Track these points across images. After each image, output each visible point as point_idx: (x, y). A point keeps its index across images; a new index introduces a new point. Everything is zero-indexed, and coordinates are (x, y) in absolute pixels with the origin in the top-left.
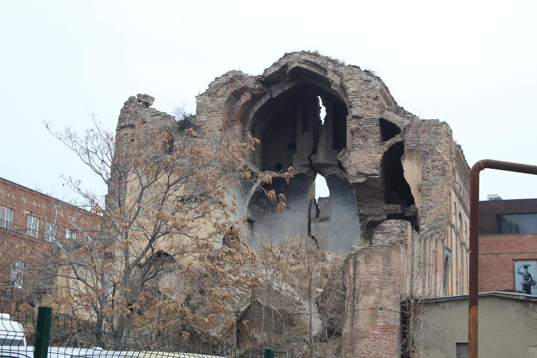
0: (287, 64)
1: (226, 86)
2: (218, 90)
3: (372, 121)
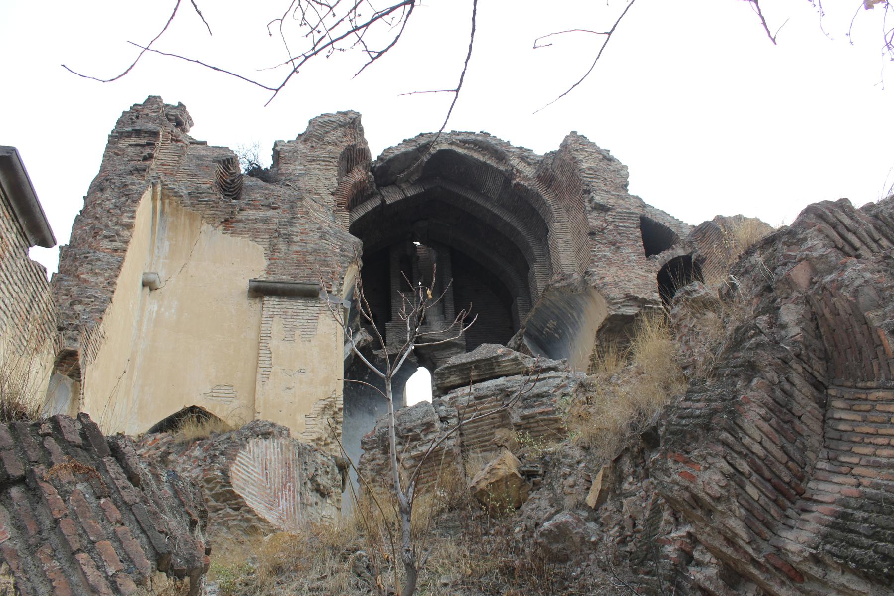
0: (428, 143)
1: (342, 129)
2: (327, 132)
3: (630, 218)
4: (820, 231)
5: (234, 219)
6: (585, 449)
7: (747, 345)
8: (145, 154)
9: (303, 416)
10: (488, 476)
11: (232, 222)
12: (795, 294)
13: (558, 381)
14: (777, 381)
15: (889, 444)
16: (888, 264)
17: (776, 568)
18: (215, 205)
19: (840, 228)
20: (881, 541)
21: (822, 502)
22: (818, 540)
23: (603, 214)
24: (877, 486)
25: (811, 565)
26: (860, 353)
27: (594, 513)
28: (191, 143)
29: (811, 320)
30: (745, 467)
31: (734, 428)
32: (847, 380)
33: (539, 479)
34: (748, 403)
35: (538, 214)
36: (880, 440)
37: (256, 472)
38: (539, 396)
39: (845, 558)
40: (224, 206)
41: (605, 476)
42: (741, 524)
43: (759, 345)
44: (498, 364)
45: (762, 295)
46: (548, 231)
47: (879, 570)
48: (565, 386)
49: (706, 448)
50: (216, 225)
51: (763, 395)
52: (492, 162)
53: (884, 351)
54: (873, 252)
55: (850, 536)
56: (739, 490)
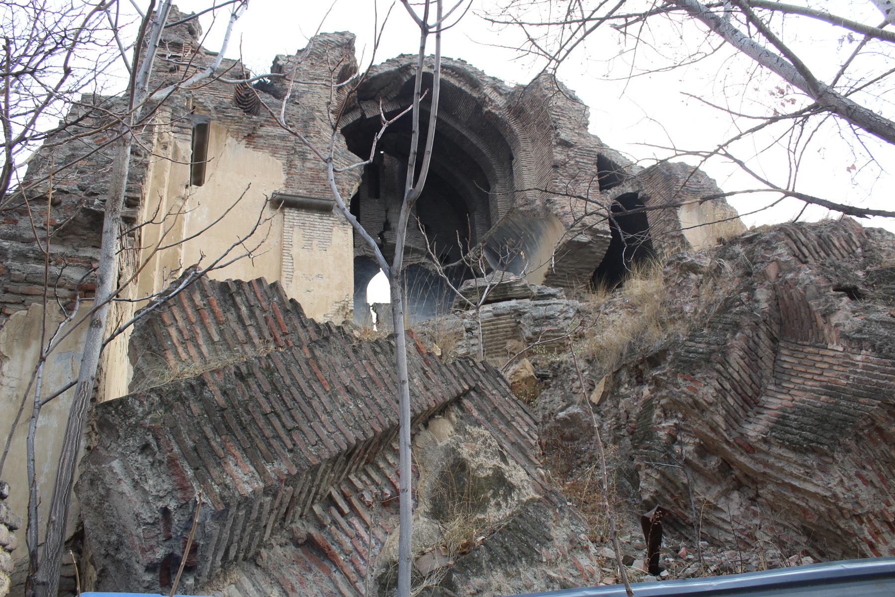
0: (409, 65)
1: (340, 49)
3: (589, 155)
4: (787, 244)
5: (256, 135)
6: (589, 362)
7: (734, 310)
9: (322, 316)
10: (513, 376)
11: (254, 137)
12: (767, 283)
13: (561, 307)
14: (751, 335)
15: (812, 379)
16: (823, 269)
17: (739, 445)
18: (239, 121)
19: (799, 243)
20: (803, 431)
21: (770, 409)
22: (767, 430)
23: (566, 150)
24: (804, 402)
25: (762, 444)
26: (802, 324)
27: (597, 407)
28: (207, 54)
29: (775, 300)
30: (727, 386)
31: (725, 362)
32: (792, 338)
33: (549, 380)
34: (733, 347)
35: (504, 139)
36: (808, 376)
38: (548, 318)
39: (783, 440)
40: (247, 122)
41: (606, 383)
42: (722, 419)
43: (742, 313)
44: (511, 289)
45: (743, 277)
46: (512, 158)
47: (802, 446)
48: (566, 311)
49: (706, 374)
50: (239, 139)
51: (742, 343)
52: (466, 89)
53: (817, 326)
54: (815, 259)
55: (786, 428)
56: (724, 400)
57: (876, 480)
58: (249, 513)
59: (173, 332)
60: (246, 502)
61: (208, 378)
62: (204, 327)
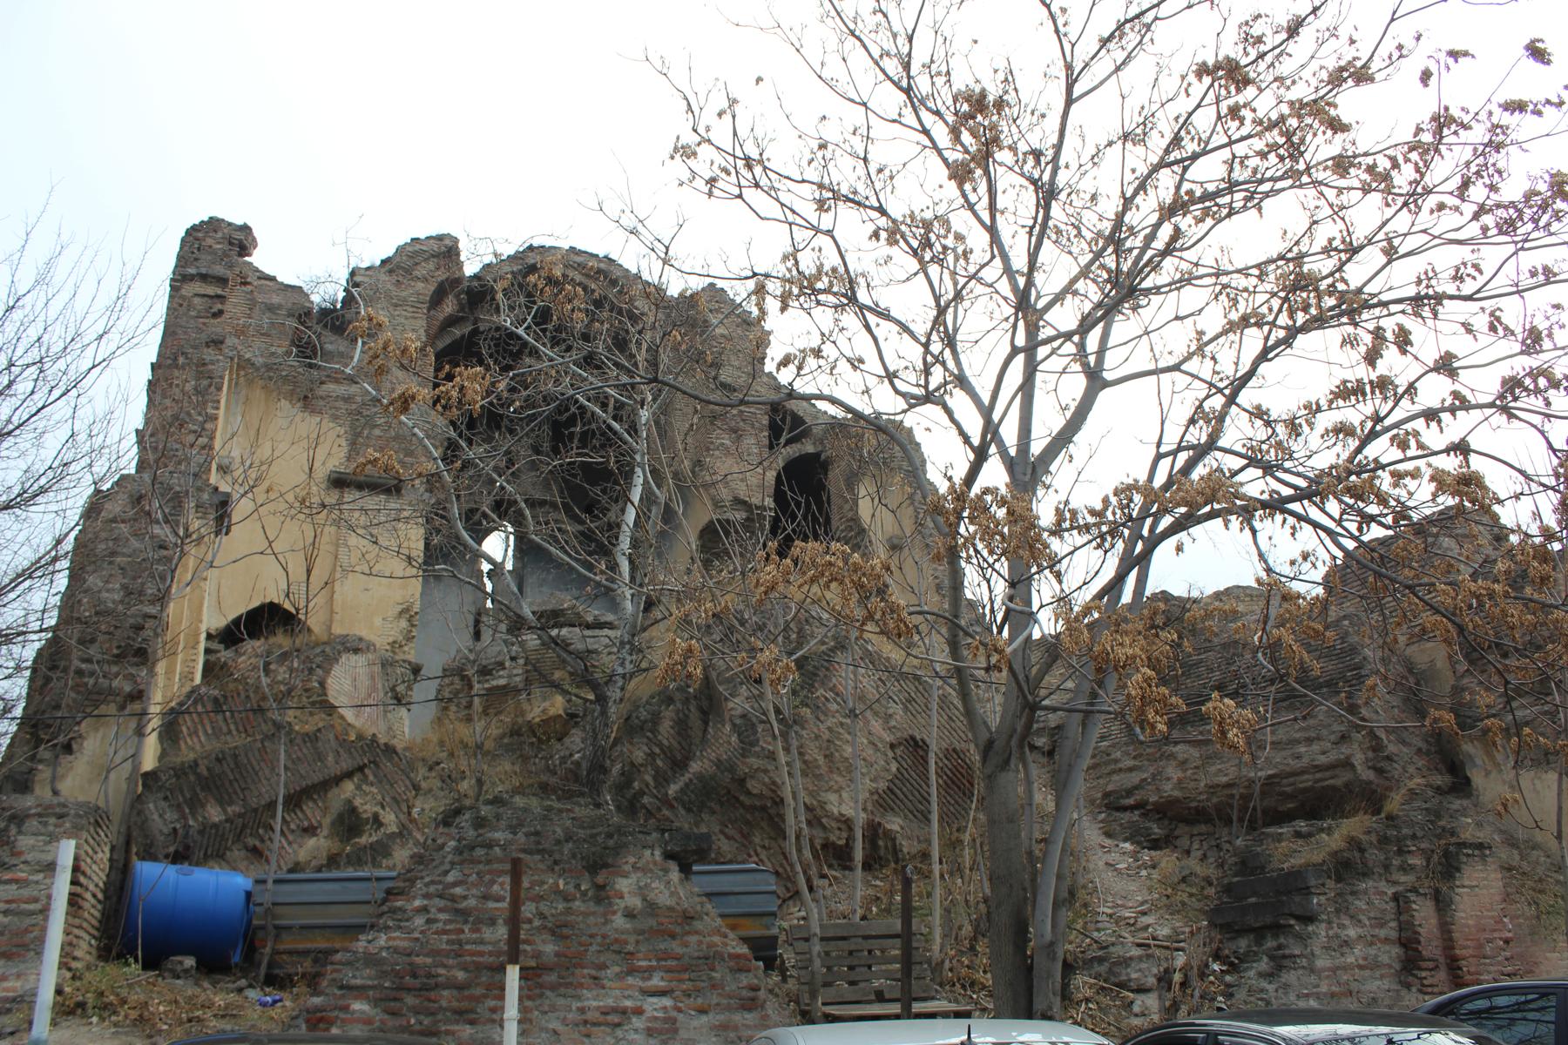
8: (215, 310)
30: (657, 750)
37: (347, 684)
51: (673, 715)
57: (737, 836)
58: (217, 830)
59: (184, 729)
60: (215, 826)
61: (200, 762)
62: (203, 725)
